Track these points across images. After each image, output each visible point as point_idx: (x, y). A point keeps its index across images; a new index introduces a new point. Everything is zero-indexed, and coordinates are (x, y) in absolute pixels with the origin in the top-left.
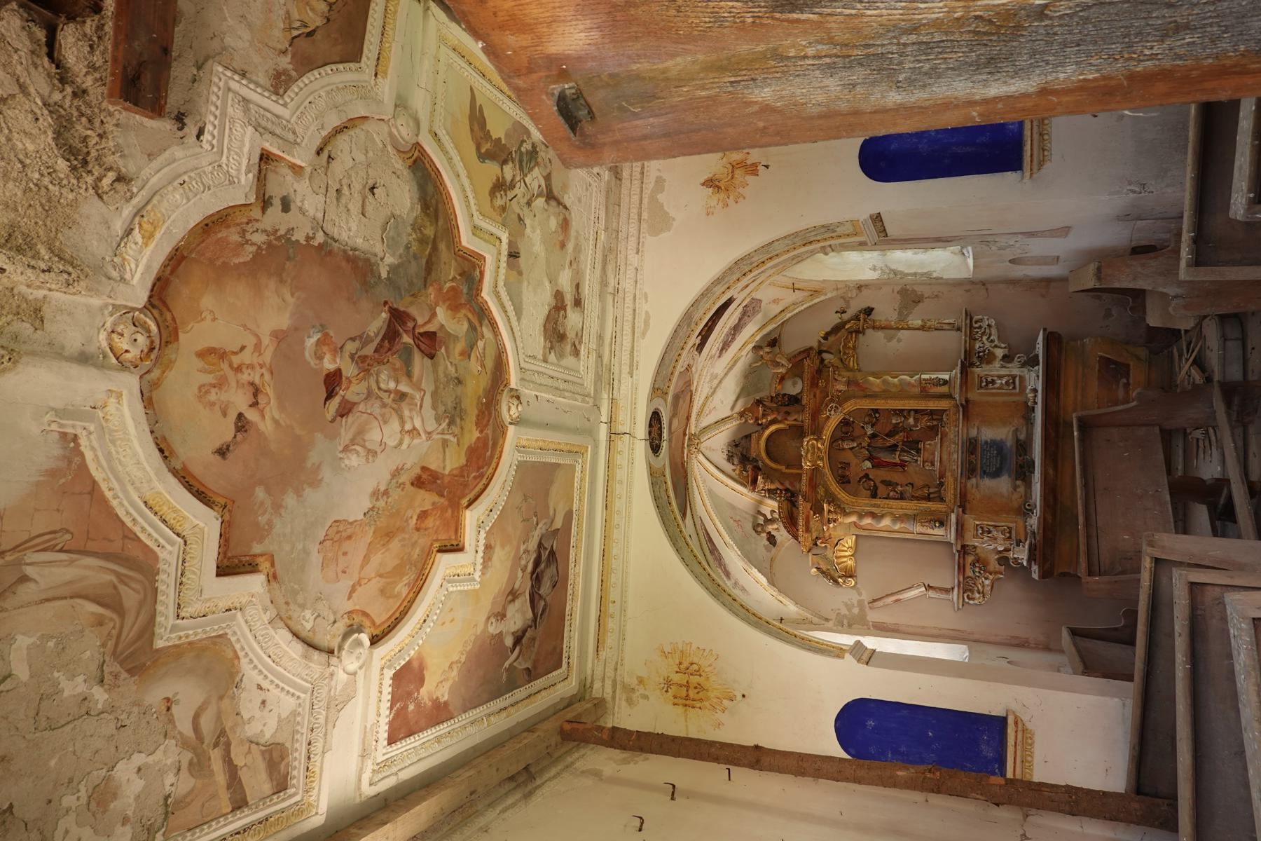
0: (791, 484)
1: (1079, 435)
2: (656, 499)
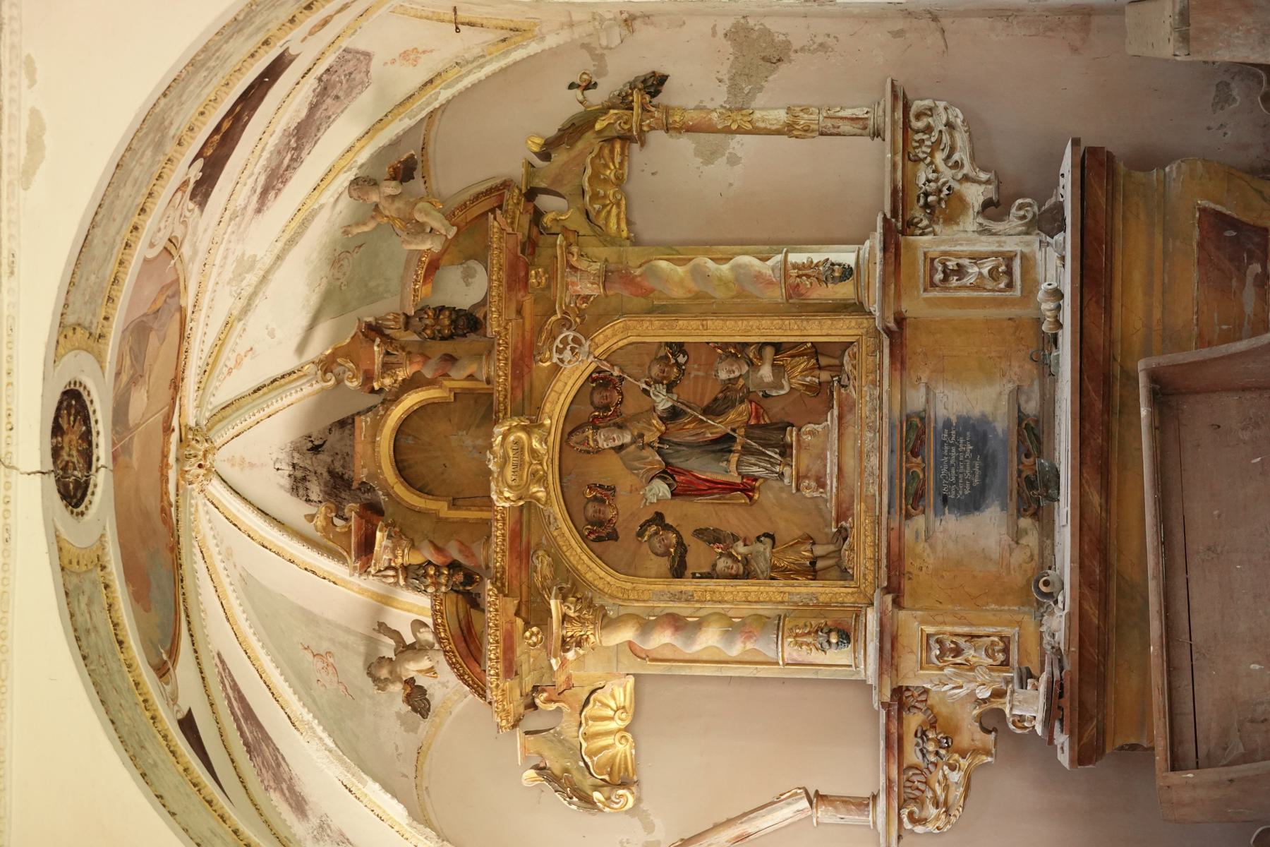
0: (465, 549)
1: (1152, 415)
2: (80, 635)
